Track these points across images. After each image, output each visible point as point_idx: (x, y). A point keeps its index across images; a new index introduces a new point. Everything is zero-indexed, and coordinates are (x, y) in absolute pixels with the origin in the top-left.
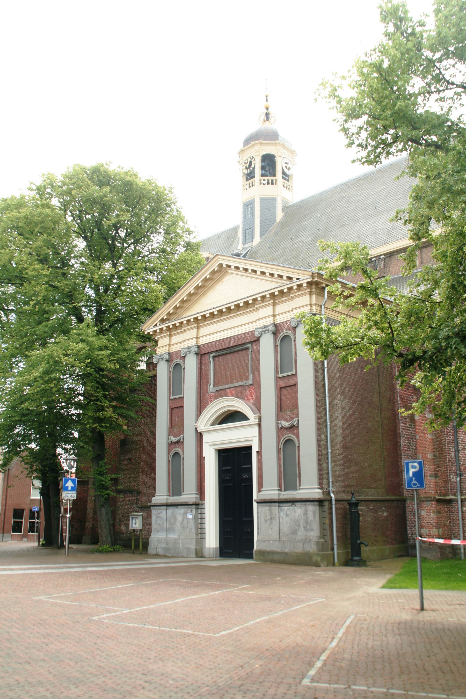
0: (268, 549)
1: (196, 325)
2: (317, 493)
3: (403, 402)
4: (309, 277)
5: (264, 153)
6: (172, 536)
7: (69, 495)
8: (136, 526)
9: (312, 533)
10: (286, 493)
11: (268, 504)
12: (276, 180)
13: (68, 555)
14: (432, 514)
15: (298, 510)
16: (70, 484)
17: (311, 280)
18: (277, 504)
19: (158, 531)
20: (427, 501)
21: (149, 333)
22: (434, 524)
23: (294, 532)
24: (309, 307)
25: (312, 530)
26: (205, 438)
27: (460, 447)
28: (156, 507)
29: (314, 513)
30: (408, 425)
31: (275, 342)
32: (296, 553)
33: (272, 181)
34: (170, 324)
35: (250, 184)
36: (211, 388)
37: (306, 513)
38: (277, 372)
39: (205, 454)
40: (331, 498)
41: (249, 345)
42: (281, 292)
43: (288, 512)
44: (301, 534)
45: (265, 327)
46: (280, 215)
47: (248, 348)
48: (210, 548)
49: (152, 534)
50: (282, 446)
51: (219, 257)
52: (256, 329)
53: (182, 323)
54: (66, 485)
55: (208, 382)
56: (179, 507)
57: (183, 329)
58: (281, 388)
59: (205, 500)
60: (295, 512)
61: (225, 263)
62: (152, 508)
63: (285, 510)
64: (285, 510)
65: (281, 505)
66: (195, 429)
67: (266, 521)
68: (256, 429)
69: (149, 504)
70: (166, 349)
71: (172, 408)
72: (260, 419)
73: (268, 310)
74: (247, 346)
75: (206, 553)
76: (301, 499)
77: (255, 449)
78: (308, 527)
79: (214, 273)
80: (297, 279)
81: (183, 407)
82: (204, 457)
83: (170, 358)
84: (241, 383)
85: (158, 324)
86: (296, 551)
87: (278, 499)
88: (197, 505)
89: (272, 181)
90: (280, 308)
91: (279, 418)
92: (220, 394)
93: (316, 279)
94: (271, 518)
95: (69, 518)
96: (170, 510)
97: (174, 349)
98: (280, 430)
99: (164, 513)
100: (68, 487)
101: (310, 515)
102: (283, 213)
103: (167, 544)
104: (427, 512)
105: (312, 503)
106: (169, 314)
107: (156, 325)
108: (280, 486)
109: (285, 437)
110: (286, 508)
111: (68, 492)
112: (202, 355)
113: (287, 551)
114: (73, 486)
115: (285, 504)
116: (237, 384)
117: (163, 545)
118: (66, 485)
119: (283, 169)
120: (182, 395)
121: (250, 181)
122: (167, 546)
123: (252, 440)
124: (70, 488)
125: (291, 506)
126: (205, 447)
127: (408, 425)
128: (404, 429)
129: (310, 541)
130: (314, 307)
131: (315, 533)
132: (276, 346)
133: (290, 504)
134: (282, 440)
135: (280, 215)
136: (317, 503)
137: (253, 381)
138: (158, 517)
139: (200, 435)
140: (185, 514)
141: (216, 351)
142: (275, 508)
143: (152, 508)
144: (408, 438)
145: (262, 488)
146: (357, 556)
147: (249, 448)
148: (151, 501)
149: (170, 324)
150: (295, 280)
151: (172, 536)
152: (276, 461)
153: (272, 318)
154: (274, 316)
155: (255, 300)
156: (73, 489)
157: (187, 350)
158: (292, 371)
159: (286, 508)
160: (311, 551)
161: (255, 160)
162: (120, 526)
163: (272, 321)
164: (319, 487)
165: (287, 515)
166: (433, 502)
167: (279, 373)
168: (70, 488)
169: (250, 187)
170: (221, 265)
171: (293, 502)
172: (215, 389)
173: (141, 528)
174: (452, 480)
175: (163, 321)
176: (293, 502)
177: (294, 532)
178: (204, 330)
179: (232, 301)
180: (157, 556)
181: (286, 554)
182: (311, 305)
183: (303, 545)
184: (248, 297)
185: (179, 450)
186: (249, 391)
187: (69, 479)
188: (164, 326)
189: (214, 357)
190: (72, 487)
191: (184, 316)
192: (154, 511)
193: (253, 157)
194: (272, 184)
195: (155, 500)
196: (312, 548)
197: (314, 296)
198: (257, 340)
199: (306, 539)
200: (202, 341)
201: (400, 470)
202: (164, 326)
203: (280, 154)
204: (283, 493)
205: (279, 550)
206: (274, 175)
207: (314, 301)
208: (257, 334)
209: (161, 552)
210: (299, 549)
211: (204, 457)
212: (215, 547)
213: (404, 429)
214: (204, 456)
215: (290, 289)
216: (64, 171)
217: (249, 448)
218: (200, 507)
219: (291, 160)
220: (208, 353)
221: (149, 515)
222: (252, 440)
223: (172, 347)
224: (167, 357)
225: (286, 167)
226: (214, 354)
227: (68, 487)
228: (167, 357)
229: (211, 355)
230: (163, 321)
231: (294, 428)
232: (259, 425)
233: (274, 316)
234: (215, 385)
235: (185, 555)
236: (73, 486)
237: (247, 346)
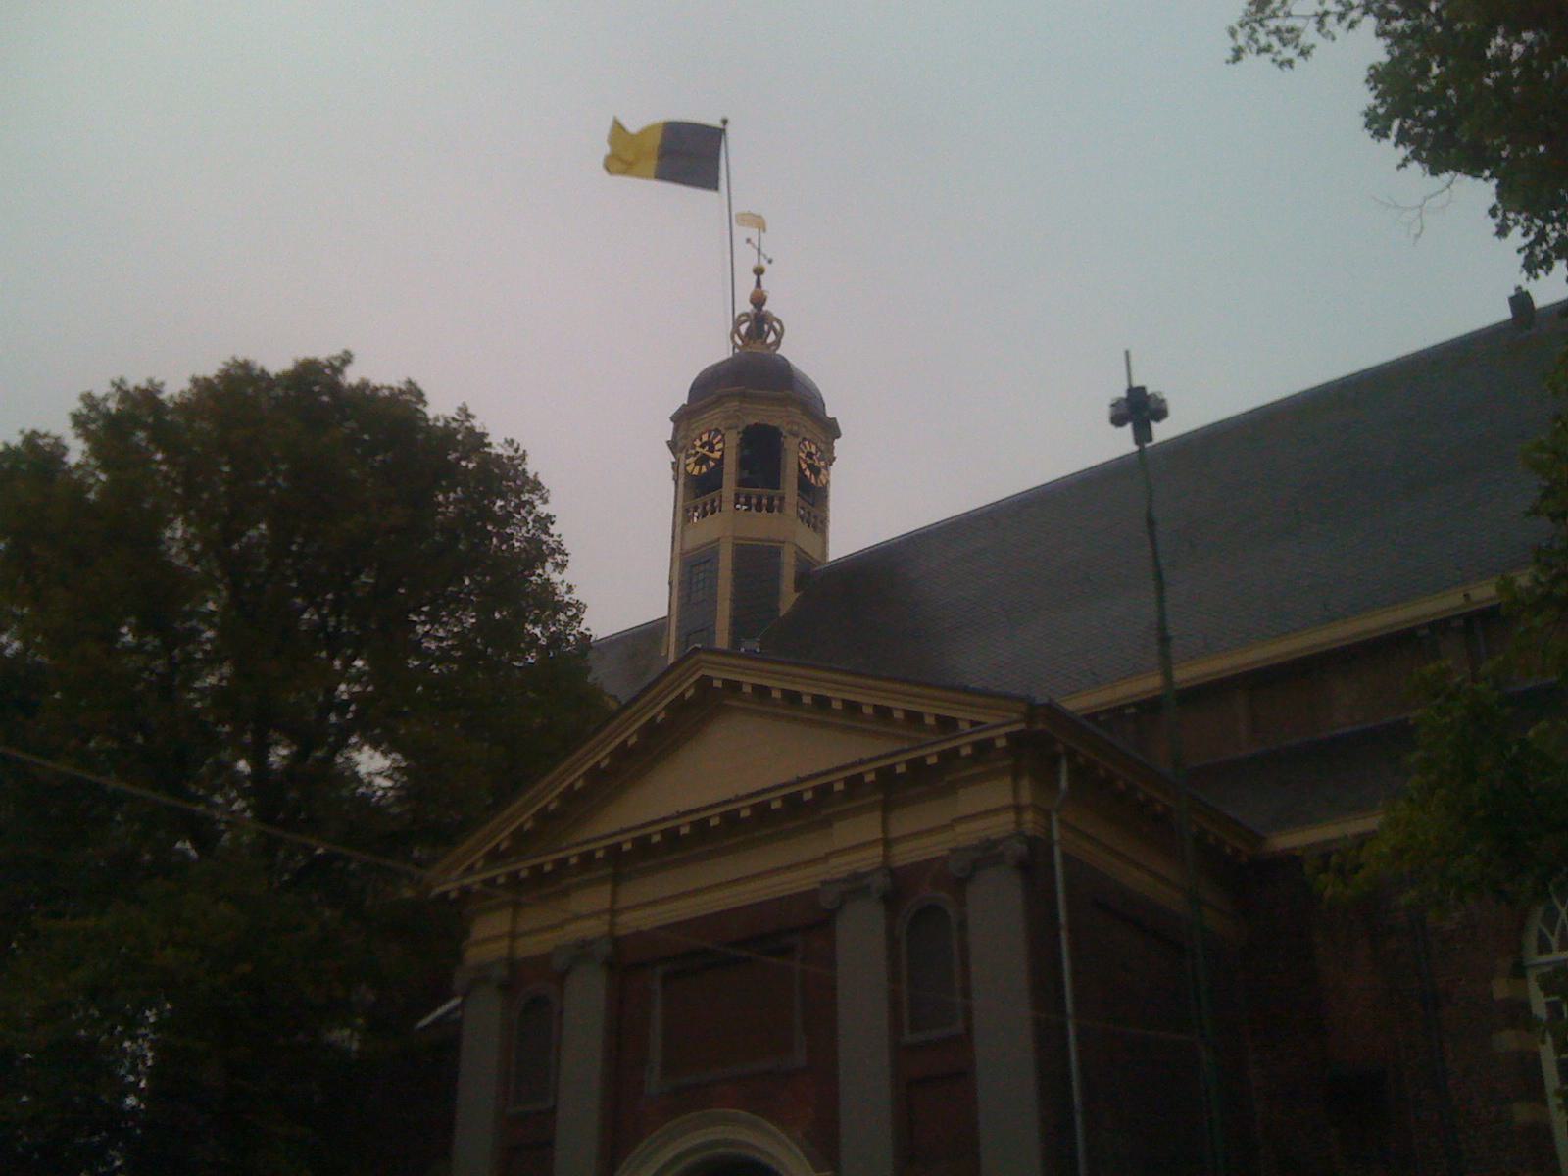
1: (880, 796)
4: (1015, 716)
5: (751, 421)
12: (782, 499)
17: (1021, 726)
21: (445, 894)
24: (1011, 816)
33: (771, 499)
35: (705, 504)
42: (917, 766)
45: (856, 877)
46: (788, 598)
51: (703, 656)
52: (824, 883)
61: (719, 678)
70: (500, 949)
73: (867, 827)
80: (973, 724)
85: (479, 865)
89: (771, 499)
90: (904, 822)
93: (1040, 726)
102: (796, 591)
119: (801, 471)
121: (708, 498)
130: (1028, 817)
135: (788, 598)
150: (965, 727)
153: (879, 850)
154: (887, 842)
155: (824, 792)
161: (722, 440)
163: (880, 859)
169: (704, 515)
170: (705, 683)
175: (495, 856)
179: (742, 792)
182: (1018, 809)
184: (800, 780)
188: (500, 873)
193: (718, 431)
194: (770, 509)
197: (1025, 783)
202: (500, 873)
203: (795, 428)
206: (776, 485)
207: (1026, 797)
215: (949, 757)
219: (823, 447)
223: (624, 919)
225: (809, 466)
230: (495, 856)
233: (887, 842)
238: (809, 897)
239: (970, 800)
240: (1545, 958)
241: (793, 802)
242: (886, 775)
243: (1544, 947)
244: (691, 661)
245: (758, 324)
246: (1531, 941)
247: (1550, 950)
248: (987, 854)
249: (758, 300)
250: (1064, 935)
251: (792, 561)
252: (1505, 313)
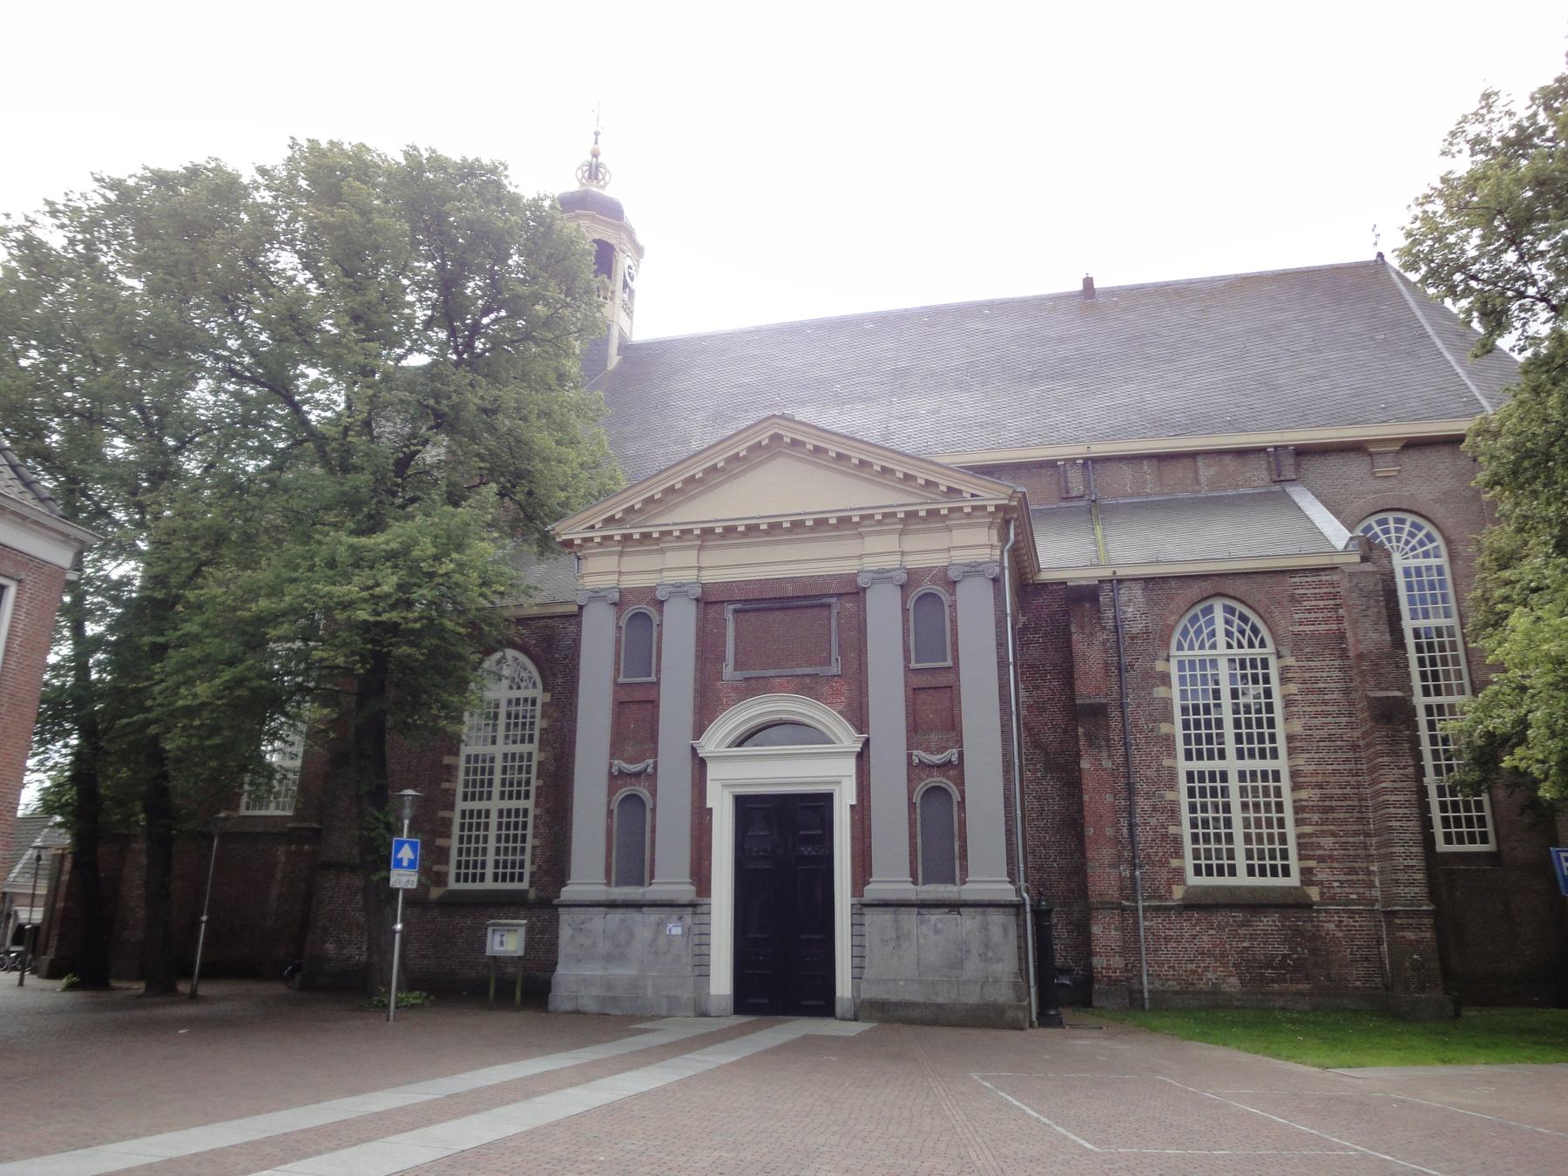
0: (894, 998)
1: (901, 526)
3: (1030, 735)
4: (1003, 496)
6: (619, 971)
7: (404, 879)
8: (502, 948)
9: (999, 967)
10: (924, 888)
11: (892, 909)
13: (395, 1020)
14: (1113, 932)
15: (968, 922)
16: (406, 853)
17: (1007, 502)
18: (915, 910)
19: (579, 961)
20: (1104, 909)
22: (1118, 949)
23: (957, 964)
25: (999, 960)
26: (713, 771)
27: (1138, 820)
28: (574, 909)
29: (1005, 929)
30: (1039, 774)
31: (904, 603)
32: (967, 1004)
36: (728, 670)
37: (985, 927)
38: (907, 659)
40: (1024, 900)
41: (833, 600)
43: (939, 926)
44: (973, 967)
46: (614, 360)
47: (829, 606)
48: (718, 996)
49: (558, 967)
50: (919, 799)
54: (399, 856)
55: (721, 658)
56: (645, 909)
57: (661, 546)
59: (709, 896)
60: (957, 925)
62: (560, 910)
63: (932, 922)
64: (932, 922)
65: (923, 911)
66: (689, 752)
67: (884, 942)
69: (556, 902)
71: (621, 703)
73: (890, 542)
74: (825, 600)
75: (713, 1010)
77: (845, 800)
78: (990, 954)
80: (973, 495)
82: (711, 809)
84: (808, 671)
86: (964, 1000)
87: (50, 879)
88: (693, 905)
92: (752, 688)
94: (898, 937)
95: (402, 932)
96: (616, 917)
99: (599, 922)
100: (401, 859)
101: (996, 932)
103: (609, 988)
104: (1104, 928)
105: (1001, 910)
106: (631, 510)
107: (592, 527)
108: (914, 874)
109: (926, 781)
110: (934, 917)
111: (402, 871)
112: (707, 603)
113: (941, 1000)
114: (412, 857)
115: (933, 910)
116: (798, 671)
117: (595, 991)
118: (399, 856)
122: (609, 994)
123: (839, 783)
124: (405, 863)
125: (949, 913)
127: (1039, 774)
128: (1030, 781)
129: (996, 981)
131: (1006, 966)
132: (905, 611)
133: (947, 910)
134: (920, 788)
136: (1013, 910)
137: (842, 670)
138: (581, 930)
139: (700, 764)
140: (661, 924)
141: (745, 601)
142: (909, 918)
143: (560, 910)
144: (1038, 799)
145: (871, 876)
148: (559, 897)
151: (619, 971)
156: (412, 864)
157: (672, 589)
158: (945, 660)
159: (934, 918)
160: (1000, 1000)
162: (324, 942)
164: (1008, 879)
165: (937, 932)
166: (1116, 912)
167: (913, 662)
168: (405, 863)
171: (955, 906)
172: (740, 675)
173: (521, 953)
174: (1123, 874)
175: (610, 520)
176: (955, 906)
177: (957, 964)
181: (940, 1006)
183: (982, 989)
185: (644, 793)
186: (832, 687)
187: (405, 842)
189: (736, 611)
190: (410, 860)
191: (657, 521)
192: (565, 917)
195: (568, 893)
196: (1002, 994)
199: (987, 977)
202: (617, 533)
205: (920, 999)
209: (591, 1006)
210: (972, 997)
211: (711, 809)
213: (1030, 781)
214: (708, 806)
216: (276, 157)
217: (827, 798)
218: (699, 910)
220: (723, 602)
221: (552, 926)
222: (839, 783)
226: (738, 606)
227: (401, 859)
229: (731, 607)
231: (955, 769)
234: (738, 666)
235: (664, 1012)
236: (412, 857)
237: (825, 600)
238: (851, 578)
239: (962, 537)
240: (1181, 653)
241: (844, 521)
242: (911, 515)
243: (1180, 647)
244: (770, 422)
245: (594, 171)
246: (1174, 644)
247: (1183, 649)
248: (973, 570)
249: (595, 155)
250: (1009, 619)
251: (617, 336)
252: (1079, 287)
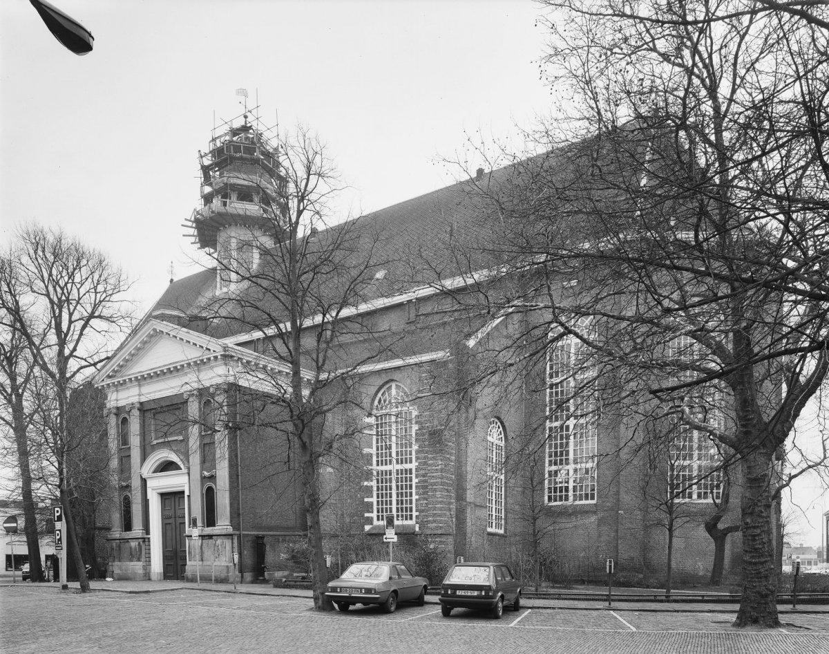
2: (230, 530)
26: (149, 484)
31: (200, 406)
34: (115, 380)
39: (149, 496)
53: (125, 381)
58: (204, 444)
68: (187, 477)
72: (189, 468)
76: (51, 5)
77: (187, 493)
79: (151, 336)
80: (214, 351)
81: (130, 456)
83: (119, 410)
91: (202, 469)
97: (121, 404)
98: (203, 478)
107: (103, 380)
112: (144, 411)
120: (128, 446)
126: (149, 491)
139: (144, 481)
146: (261, 576)
147: (183, 492)
149: (115, 380)
152: (200, 500)
170: (155, 330)
175: (109, 377)
178: (145, 389)
180: (193, 580)
198: (186, 402)
200: (143, 399)
201: (553, 162)
204: (206, 529)
208: (185, 396)
212: (159, 571)
217: (183, 492)
224: (115, 411)
228: (115, 411)
232: (189, 474)
